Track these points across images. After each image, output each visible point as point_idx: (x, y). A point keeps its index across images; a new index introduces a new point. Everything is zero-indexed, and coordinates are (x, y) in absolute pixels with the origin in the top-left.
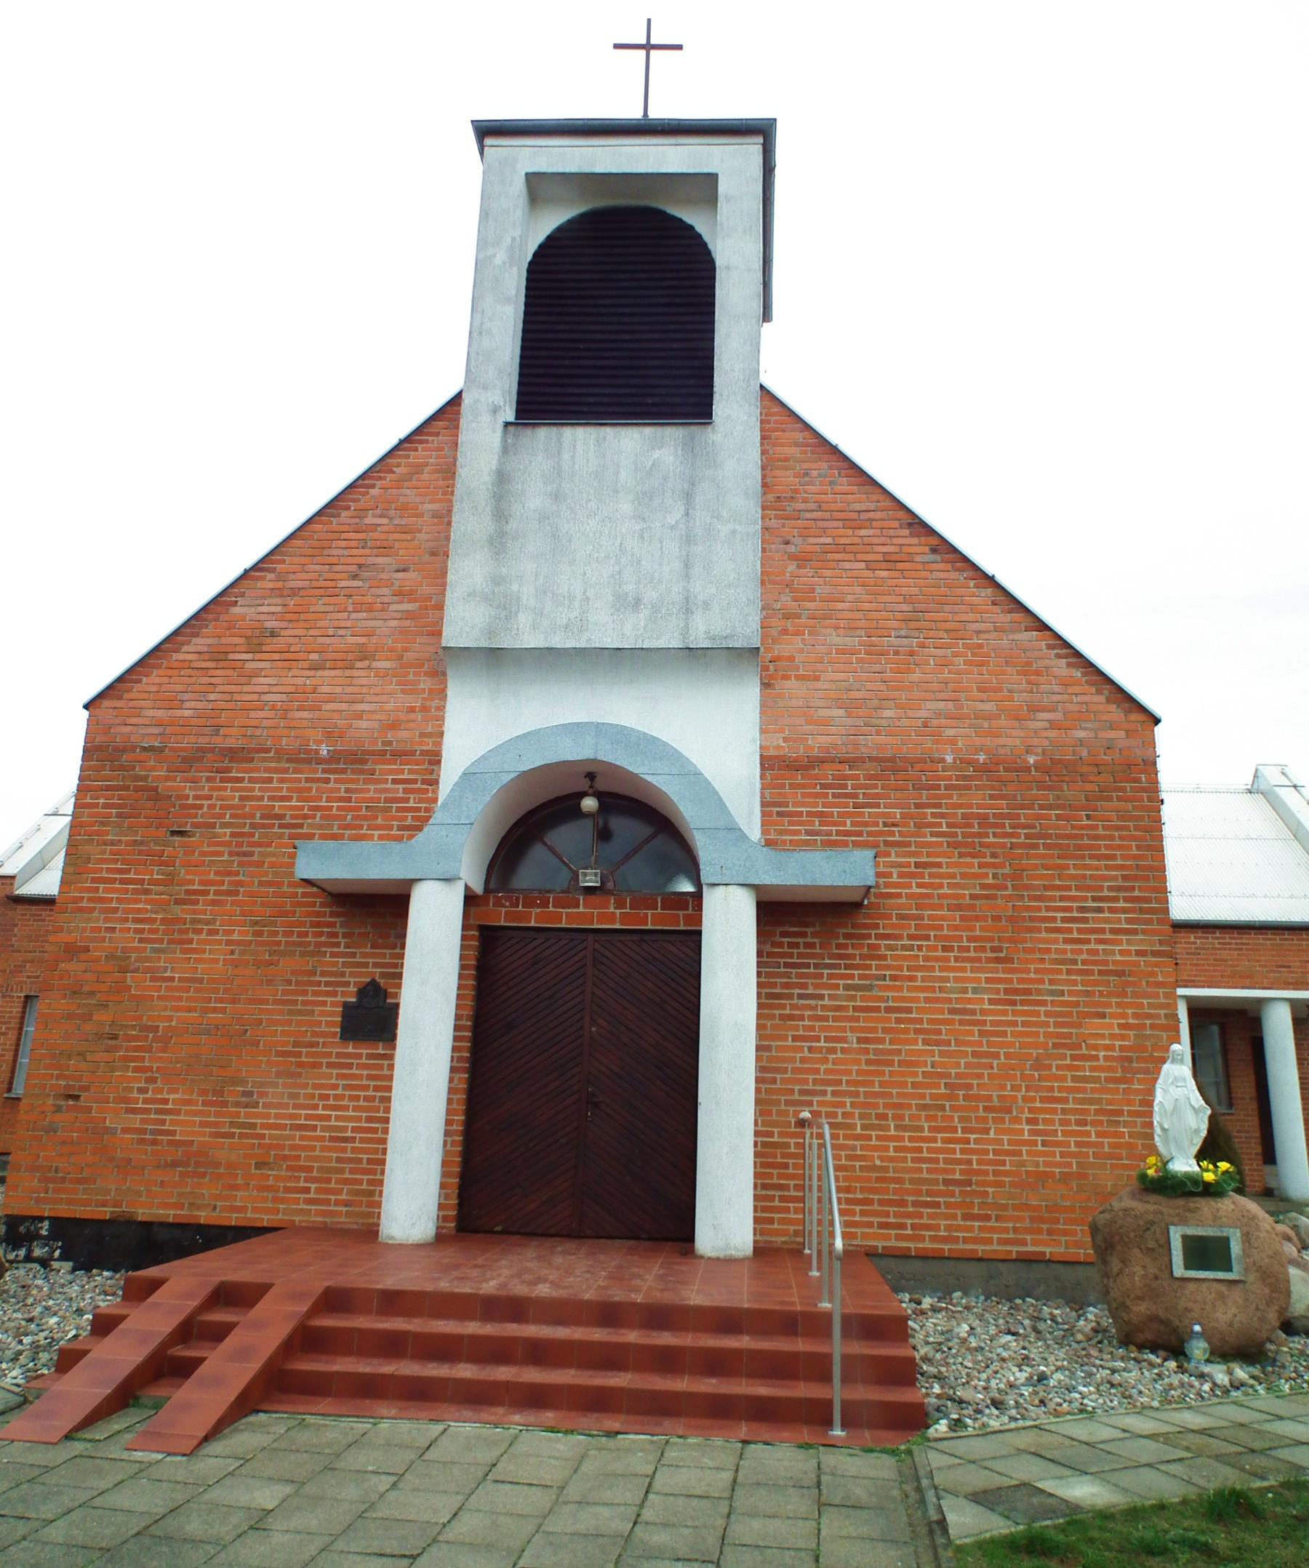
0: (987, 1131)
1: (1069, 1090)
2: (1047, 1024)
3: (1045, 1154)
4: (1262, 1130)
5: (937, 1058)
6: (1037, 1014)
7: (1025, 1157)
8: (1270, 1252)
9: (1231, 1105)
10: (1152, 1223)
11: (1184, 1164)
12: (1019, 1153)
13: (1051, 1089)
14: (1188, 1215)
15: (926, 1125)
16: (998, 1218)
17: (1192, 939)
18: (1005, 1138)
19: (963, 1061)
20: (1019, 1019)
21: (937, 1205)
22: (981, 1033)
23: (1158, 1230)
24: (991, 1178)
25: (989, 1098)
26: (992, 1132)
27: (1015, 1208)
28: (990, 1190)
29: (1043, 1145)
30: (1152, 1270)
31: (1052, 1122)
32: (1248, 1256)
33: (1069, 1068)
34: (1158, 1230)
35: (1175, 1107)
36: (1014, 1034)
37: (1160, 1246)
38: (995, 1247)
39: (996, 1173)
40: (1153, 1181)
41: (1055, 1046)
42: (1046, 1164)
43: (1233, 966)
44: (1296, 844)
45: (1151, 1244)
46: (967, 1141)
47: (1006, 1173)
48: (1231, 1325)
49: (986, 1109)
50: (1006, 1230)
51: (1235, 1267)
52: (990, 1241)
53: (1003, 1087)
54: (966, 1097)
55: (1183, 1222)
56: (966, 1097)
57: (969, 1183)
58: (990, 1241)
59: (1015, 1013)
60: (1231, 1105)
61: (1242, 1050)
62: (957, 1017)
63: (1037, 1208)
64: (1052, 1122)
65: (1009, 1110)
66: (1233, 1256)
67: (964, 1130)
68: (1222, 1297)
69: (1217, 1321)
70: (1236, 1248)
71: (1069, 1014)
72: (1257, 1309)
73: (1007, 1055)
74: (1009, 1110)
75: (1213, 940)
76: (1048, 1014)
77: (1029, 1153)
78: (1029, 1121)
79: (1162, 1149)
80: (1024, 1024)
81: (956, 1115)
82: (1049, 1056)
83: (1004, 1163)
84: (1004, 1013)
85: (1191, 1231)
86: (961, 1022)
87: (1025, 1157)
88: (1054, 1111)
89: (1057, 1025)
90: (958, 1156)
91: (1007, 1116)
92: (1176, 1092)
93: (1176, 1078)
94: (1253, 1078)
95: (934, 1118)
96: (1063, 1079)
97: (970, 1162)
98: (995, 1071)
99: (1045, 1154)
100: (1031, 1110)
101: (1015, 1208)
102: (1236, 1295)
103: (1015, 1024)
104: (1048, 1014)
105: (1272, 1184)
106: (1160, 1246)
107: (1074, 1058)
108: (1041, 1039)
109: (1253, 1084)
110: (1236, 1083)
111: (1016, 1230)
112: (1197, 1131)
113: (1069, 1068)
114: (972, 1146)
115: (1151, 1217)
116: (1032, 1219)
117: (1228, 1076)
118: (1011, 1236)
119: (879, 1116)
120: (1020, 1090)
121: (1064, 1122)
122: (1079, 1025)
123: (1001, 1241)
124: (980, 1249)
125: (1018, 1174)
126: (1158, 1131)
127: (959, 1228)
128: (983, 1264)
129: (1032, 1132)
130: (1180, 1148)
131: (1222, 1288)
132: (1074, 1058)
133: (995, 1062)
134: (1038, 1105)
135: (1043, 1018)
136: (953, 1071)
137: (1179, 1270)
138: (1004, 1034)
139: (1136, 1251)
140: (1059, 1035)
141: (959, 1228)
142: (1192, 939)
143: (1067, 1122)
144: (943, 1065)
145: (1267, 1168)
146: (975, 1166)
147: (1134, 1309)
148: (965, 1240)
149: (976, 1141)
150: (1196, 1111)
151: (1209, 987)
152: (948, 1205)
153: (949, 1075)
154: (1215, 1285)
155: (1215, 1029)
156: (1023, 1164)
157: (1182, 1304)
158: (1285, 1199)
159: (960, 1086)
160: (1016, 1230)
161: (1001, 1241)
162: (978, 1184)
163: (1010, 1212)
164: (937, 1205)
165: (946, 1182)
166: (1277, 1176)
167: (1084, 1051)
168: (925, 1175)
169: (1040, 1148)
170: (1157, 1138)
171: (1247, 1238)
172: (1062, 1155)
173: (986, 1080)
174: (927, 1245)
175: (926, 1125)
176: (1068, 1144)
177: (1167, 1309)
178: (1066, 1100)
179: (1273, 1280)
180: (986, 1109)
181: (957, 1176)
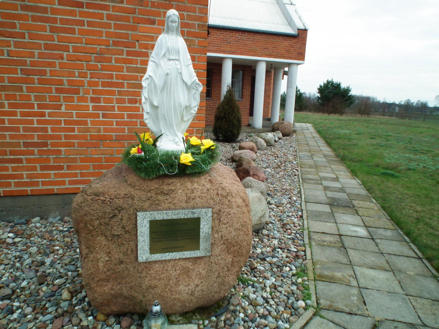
0: (59, 107)
1: (124, 78)
2: (108, 26)
3: (104, 123)
4: (251, 88)
5: (12, 48)
6: (101, 16)
7: (89, 126)
8: (238, 226)
9: (242, 98)
10: (120, 209)
11: (171, 143)
12: (86, 123)
13: (111, 76)
14: (160, 197)
15: (6, 102)
16: (69, 168)
17: (237, 36)
18: (74, 112)
19: (36, 52)
20: (86, 20)
21: (20, 161)
22: (52, 30)
23: (126, 217)
24: (63, 140)
25: (61, 82)
26: (63, 108)
27: (82, 160)
28: (63, 149)
29: (103, 117)
30: (117, 255)
31: (111, 101)
32: (217, 232)
33: (125, 61)
34: (126, 217)
35: (165, 83)
36: (81, 32)
37: (127, 232)
38: (67, 186)
39: (66, 137)
40: (139, 160)
41: (115, 43)
42: (105, 130)
43: (250, 47)
44: (277, 6)
45: (118, 231)
46: (43, 115)
47: (75, 137)
48: (192, 294)
49: (58, 91)
50: (76, 175)
51: (203, 244)
52: (63, 183)
53: (72, 74)
54: (40, 81)
55: (155, 206)
56: (40, 81)
57: (46, 145)
58: (63, 183)
59: (82, 14)
60: (242, 98)
61: (248, 80)
62: (30, 14)
63: (99, 160)
64: (111, 101)
65: (77, 92)
66: (202, 235)
67: (39, 107)
68: (186, 272)
69: (180, 293)
70: (205, 228)
71: (127, 19)
72: (219, 276)
73: (76, 50)
74: (77, 92)
75: (244, 36)
76: (109, 17)
77: (92, 123)
78: (93, 100)
79: (150, 124)
80: (90, 24)
81: (32, 95)
82: (109, 51)
83: (73, 130)
84: (73, 13)
85: (160, 216)
86: (34, 19)
87: (89, 126)
88: (112, 93)
89: (117, 27)
90: (35, 125)
91: (76, 96)
92: (167, 66)
93: (168, 50)
94: (250, 88)
95: (14, 97)
96: (120, 69)
97: (46, 130)
98: (65, 61)
99: (104, 123)
100: (94, 92)
101: (82, 160)
102: (201, 269)
103: (82, 23)
104: (109, 17)
105: (251, 123)
106: (127, 232)
107: (129, 53)
108: (104, 38)
109: (250, 91)
110: (245, 90)
111: (82, 175)
112: (188, 108)
113: (125, 61)
114: (47, 118)
115: (120, 202)
116: (95, 167)
117: (243, 88)
118: (79, 178)
119: (52, 99)
120: (86, 77)
121: (119, 101)
122: (134, 29)
123: (71, 183)
124: (55, 188)
125: (85, 137)
126: (147, 107)
127: (38, 176)
128: (60, 197)
129: (94, 108)
130: (170, 126)
131: (189, 264)
132: (129, 53)
133: (65, 54)
134: (100, 88)
135: (105, 20)
136: (28, 60)
137: (144, 253)
138: (73, 31)
139: (101, 239)
140: (117, 35)
141: (38, 176)
142: (237, 36)
143: (123, 101)
144: (18, 54)
145: (250, 118)
146: (50, 133)
147: (98, 289)
148: (44, 183)
149: (50, 115)
150: (188, 88)
151: (241, 55)
152: (28, 161)
153: (24, 63)
154: (182, 263)
155: (241, 72)
156: (88, 130)
157: (146, 283)
158: (254, 128)
159: (35, 73)
160: (82, 175)
161: (71, 183)
162: (53, 145)
163: (79, 164)
164: (20, 161)
165: (26, 145)
166: (252, 120)
167: (137, 49)
168: (8, 140)
169: (101, 119)
170: (145, 116)
171: (217, 216)
172: (118, 123)
173: (58, 68)
174: (13, 188)
175: (6, 102)
176: (122, 116)
177: (131, 288)
178: (122, 85)
179: (236, 248)
180: (58, 91)
181: (36, 140)
